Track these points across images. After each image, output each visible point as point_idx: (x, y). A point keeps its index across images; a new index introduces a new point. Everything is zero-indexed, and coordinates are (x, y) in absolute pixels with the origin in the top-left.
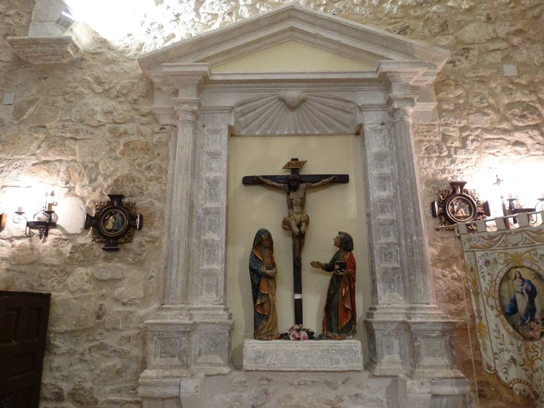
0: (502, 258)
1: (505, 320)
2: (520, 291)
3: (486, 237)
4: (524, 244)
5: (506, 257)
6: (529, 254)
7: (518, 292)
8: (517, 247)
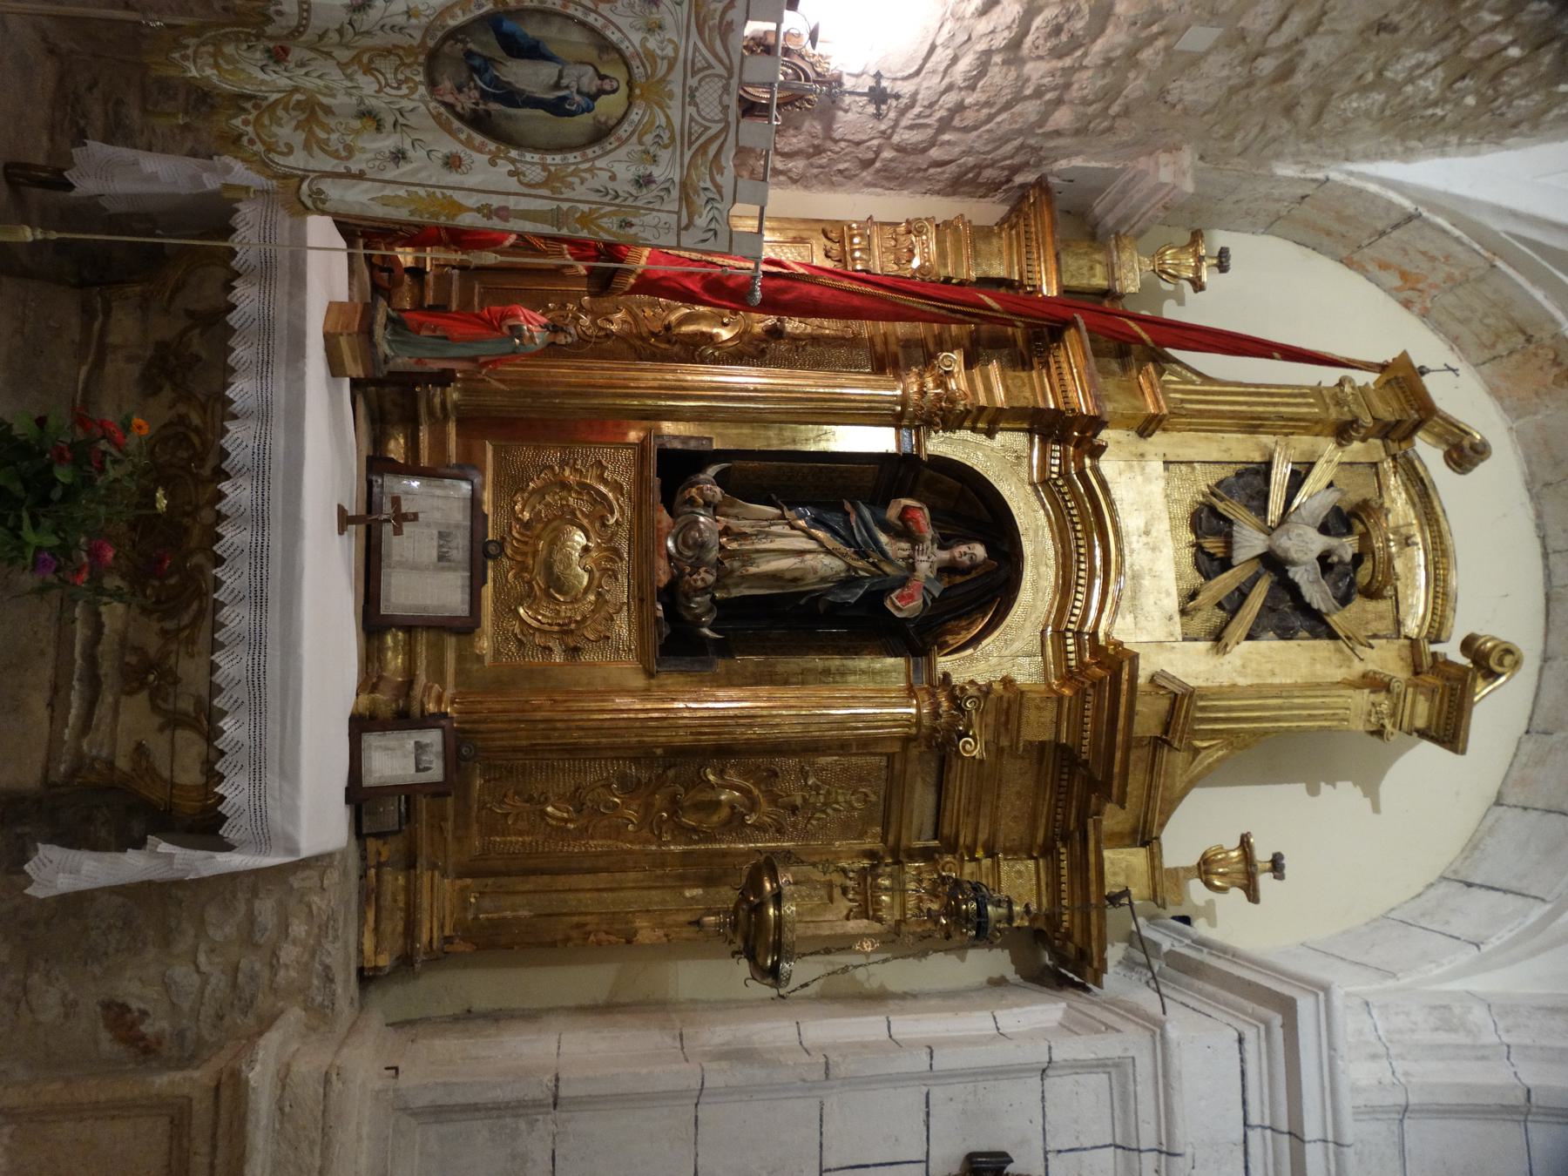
0: (663, 50)
1: (478, 12)
2: (564, 82)
3: (730, 15)
4: (692, 119)
5: (663, 58)
6: (664, 125)
7: (560, 76)
8: (688, 100)
